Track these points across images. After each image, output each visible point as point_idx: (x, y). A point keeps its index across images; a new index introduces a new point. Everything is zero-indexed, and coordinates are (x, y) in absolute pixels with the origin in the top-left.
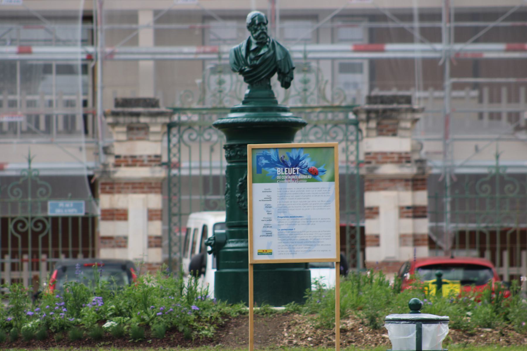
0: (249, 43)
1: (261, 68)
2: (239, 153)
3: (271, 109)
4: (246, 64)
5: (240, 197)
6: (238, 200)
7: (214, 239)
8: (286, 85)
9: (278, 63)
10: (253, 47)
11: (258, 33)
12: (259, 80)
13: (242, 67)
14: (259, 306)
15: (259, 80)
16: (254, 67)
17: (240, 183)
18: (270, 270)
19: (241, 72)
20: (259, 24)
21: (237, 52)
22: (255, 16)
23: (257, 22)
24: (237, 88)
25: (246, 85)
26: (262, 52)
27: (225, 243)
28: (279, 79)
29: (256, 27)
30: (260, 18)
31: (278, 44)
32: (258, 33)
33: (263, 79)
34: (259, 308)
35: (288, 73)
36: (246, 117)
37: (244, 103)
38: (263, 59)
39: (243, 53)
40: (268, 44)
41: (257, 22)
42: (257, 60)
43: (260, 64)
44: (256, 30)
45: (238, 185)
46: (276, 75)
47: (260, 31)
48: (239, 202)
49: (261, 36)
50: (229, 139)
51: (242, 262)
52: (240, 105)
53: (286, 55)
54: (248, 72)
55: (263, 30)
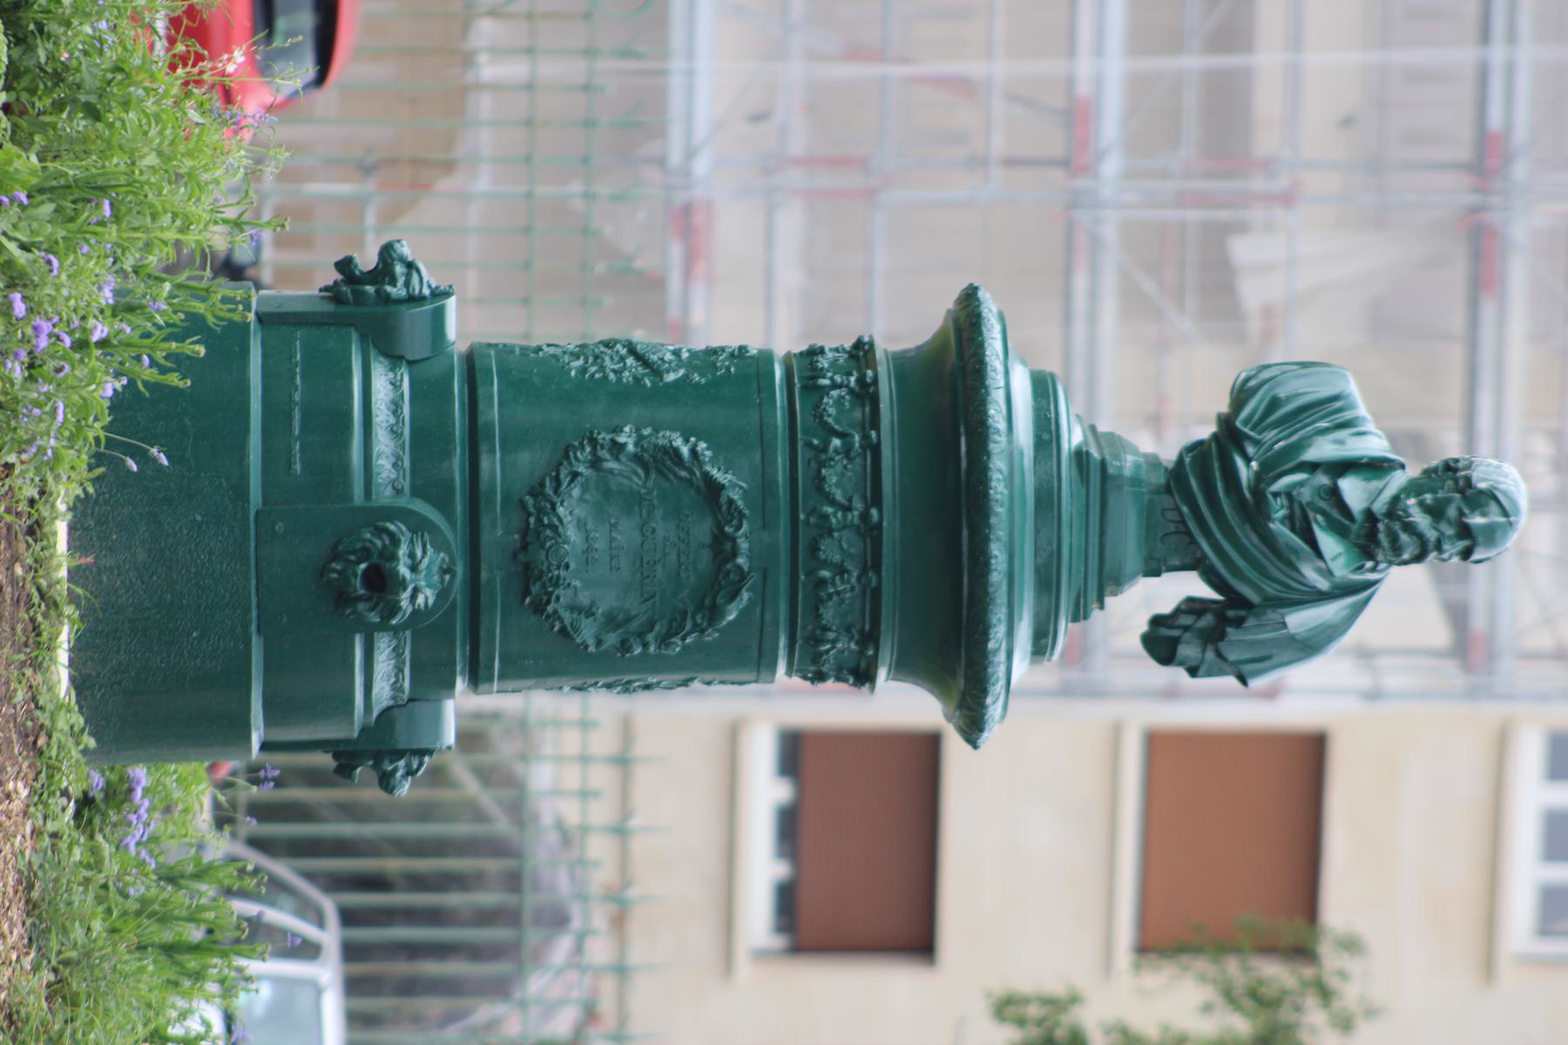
0: (1376, 467)
1: (1250, 539)
2: (836, 442)
3: (1047, 583)
4: (1272, 467)
5: (617, 448)
6: (604, 437)
7: (414, 299)
8: (1162, 641)
9: (1272, 615)
10: (1353, 490)
11: (1421, 520)
12: (1192, 526)
13: (1256, 443)
14: (74, 575)
15: (1192, 526)
16: (1254, 509)
17: (685, 451)
18: (254, 614)
19: (1229, 436)
20: (1465, 532)
21: (1329, 411)
22: (1505, 513)
23: (1477, 520)
24: (1146, 399)
25: (1169, 454)
26: (1329, 543)
27: (395, 359)
28: (1193, 606)
29: (1452, 512)
30: (1492, 535)
31: (1367, 601)
32: (1421, 520)
33: (1193, 541)
34: (63, 573)
35: (1220, 655)
36: (1012, 455)
37: (1081, 456)
38: (1296, 551)
39: (1324, 449)
40: (1369, 564)
41: (1477, 520)
42: (1290, 520)
43: (1268, 539)
44: (1436, 512)
45: (678, 442)
46: (1204, 591)
47: (1432, 535)
48: (593, 442)
49: (1404, 537)
50: (903, 364)
51: (298, 467)
52: (1073, 437)
53: (1309, 646)
54: (1231, 475)
55: (1439, 547)
